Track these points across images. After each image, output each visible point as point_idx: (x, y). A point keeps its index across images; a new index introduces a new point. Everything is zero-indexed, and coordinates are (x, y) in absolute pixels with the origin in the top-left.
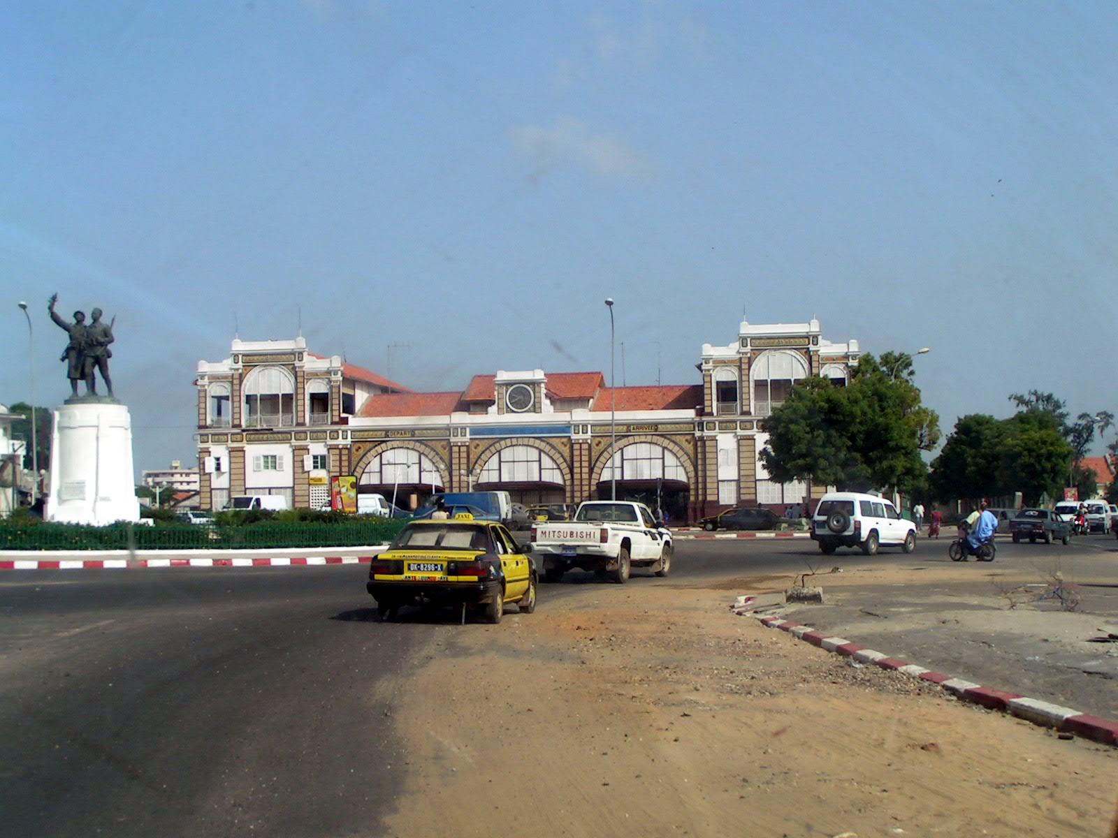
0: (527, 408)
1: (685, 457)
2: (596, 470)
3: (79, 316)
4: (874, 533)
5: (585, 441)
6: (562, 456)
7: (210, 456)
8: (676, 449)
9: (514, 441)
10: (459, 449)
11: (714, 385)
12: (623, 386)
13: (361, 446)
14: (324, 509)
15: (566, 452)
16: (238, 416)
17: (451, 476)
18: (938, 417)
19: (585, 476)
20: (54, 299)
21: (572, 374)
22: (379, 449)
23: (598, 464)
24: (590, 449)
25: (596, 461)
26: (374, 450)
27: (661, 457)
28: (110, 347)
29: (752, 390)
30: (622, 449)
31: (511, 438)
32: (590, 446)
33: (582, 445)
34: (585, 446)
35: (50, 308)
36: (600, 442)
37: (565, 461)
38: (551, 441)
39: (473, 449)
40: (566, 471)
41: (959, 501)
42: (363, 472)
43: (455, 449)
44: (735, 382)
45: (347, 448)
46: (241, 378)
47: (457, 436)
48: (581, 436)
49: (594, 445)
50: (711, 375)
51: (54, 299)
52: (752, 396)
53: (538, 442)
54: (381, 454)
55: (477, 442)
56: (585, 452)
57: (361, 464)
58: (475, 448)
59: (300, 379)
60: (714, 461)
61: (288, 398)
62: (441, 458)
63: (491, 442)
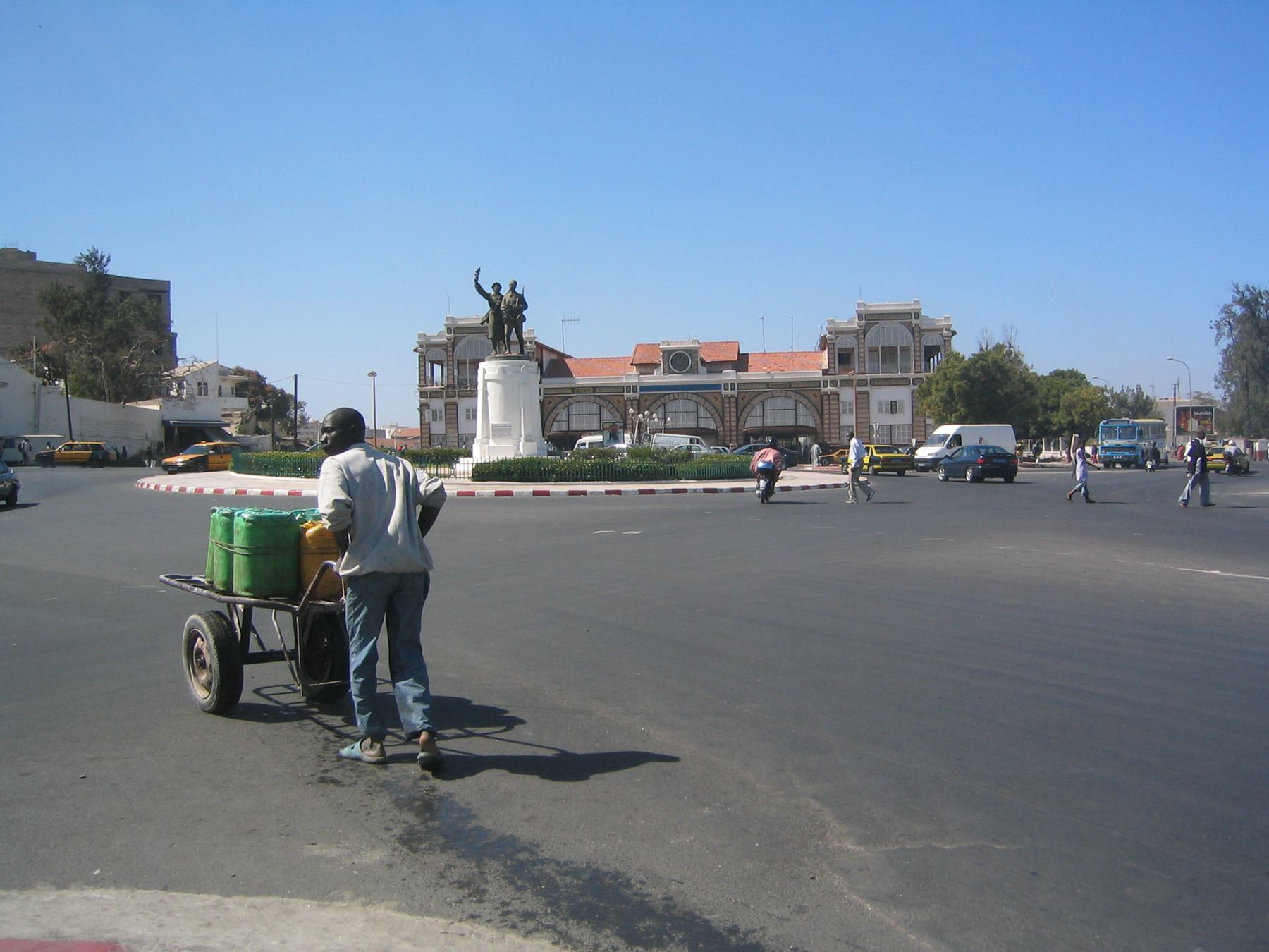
0: (686, 370)
1: (813, 408)
2: (741, 418)
3: (497, 287)
4: (157, 487)
5: (635, 399)
6: (715, 408)
7: (429, 408)
8: (805, 401)
9: (775, 394)
10: (730, 400)
11: (923, 349)
12: (762, 352)
13: (818, 398)
14: (544, 457)
15: (719, 406)
16: (863, 365)
17: (822, 423)
18: (282, 389)
19: (734, 424)
20: (478, 271)
21: (716, 343)
22: (566, 403)
23: (744, 414)
24: (737, 402)
25: (742, 412)
26: (562, 404)
27: (794, 408)
28: (524, 313)
29: (867, 355)
30: (762, 402)
31: (673, 393)
32: (737, 399)
33: (831, 396)
34: (733, 400)
35: (476, 280)
36: (744, 397)
37: (717, 411)
38: (705, 396)
39: (643, 402)
40: (718, 419)
41: (1043, 439)
42: (748, 416)
43: (825, 398)
44: (853, 349)
45: (630, 400)
46: (453, 345)
47: (630, 392)
48: (729, 392)
49: (740, 399)
50: (834, 344)
51: (478, 271)
52: (867, 359)
53: (695, 396)
54: (568, 407)
55: (744, 394)
56: (733, 405)
57: (552, 415)
58: (743, 399)
59: (917, 334)
60: (837, 411)
61: (905, 350)
62: (617, 410)
63: (754, 394)
